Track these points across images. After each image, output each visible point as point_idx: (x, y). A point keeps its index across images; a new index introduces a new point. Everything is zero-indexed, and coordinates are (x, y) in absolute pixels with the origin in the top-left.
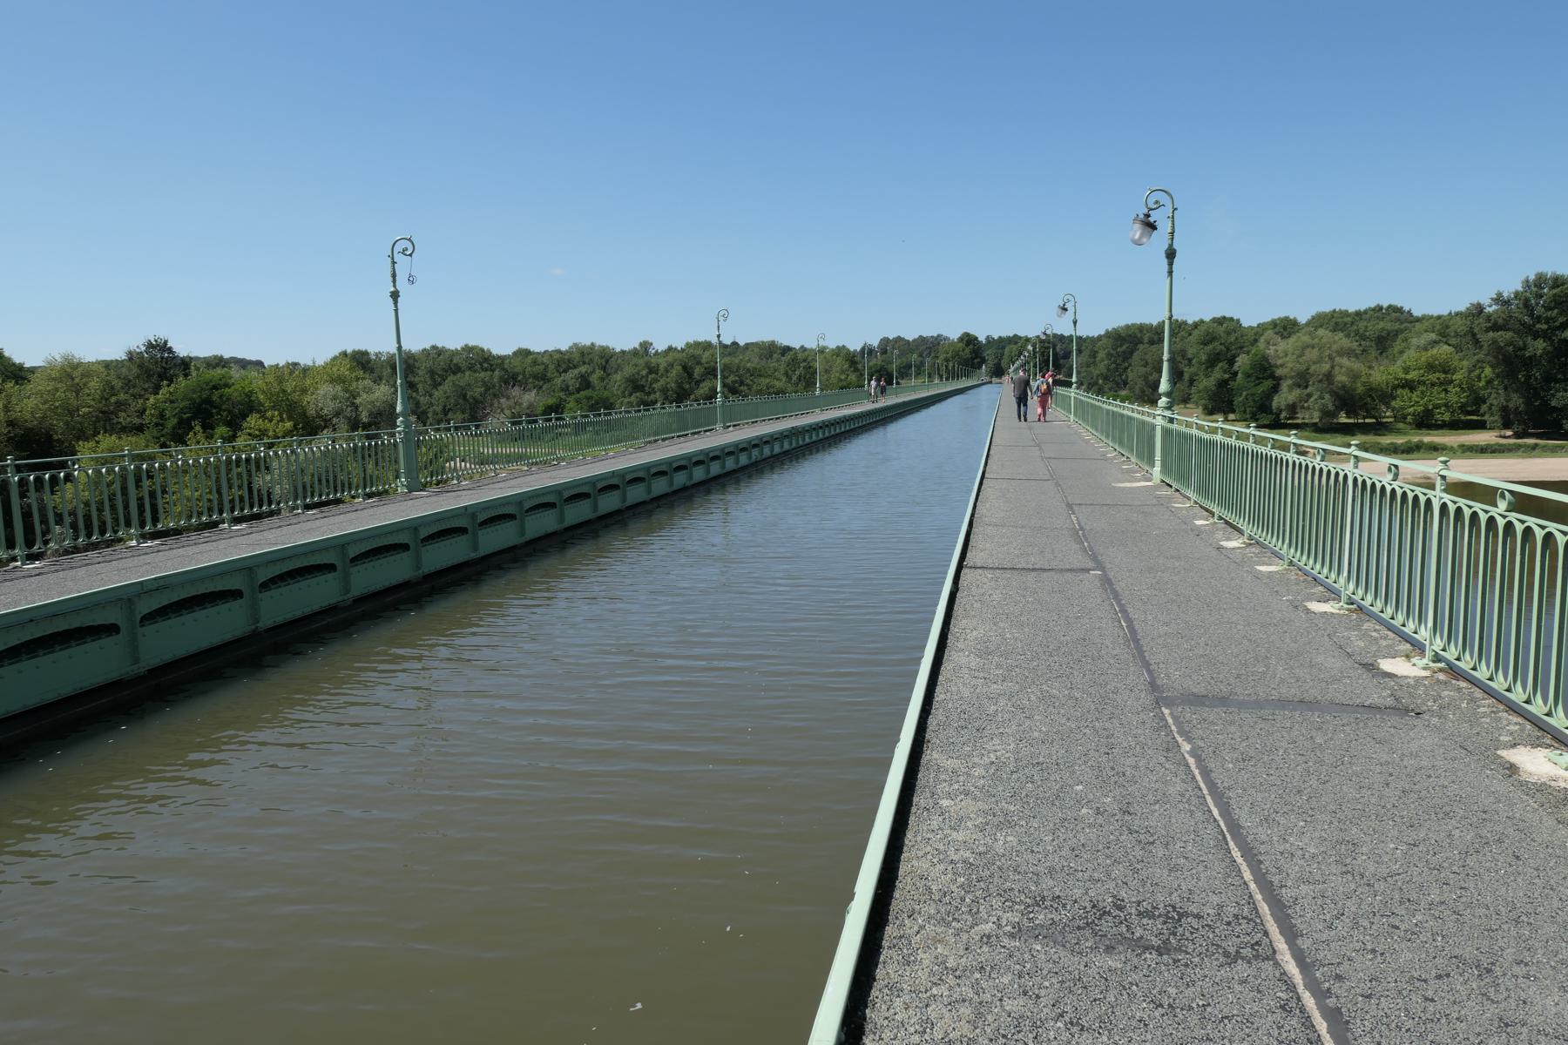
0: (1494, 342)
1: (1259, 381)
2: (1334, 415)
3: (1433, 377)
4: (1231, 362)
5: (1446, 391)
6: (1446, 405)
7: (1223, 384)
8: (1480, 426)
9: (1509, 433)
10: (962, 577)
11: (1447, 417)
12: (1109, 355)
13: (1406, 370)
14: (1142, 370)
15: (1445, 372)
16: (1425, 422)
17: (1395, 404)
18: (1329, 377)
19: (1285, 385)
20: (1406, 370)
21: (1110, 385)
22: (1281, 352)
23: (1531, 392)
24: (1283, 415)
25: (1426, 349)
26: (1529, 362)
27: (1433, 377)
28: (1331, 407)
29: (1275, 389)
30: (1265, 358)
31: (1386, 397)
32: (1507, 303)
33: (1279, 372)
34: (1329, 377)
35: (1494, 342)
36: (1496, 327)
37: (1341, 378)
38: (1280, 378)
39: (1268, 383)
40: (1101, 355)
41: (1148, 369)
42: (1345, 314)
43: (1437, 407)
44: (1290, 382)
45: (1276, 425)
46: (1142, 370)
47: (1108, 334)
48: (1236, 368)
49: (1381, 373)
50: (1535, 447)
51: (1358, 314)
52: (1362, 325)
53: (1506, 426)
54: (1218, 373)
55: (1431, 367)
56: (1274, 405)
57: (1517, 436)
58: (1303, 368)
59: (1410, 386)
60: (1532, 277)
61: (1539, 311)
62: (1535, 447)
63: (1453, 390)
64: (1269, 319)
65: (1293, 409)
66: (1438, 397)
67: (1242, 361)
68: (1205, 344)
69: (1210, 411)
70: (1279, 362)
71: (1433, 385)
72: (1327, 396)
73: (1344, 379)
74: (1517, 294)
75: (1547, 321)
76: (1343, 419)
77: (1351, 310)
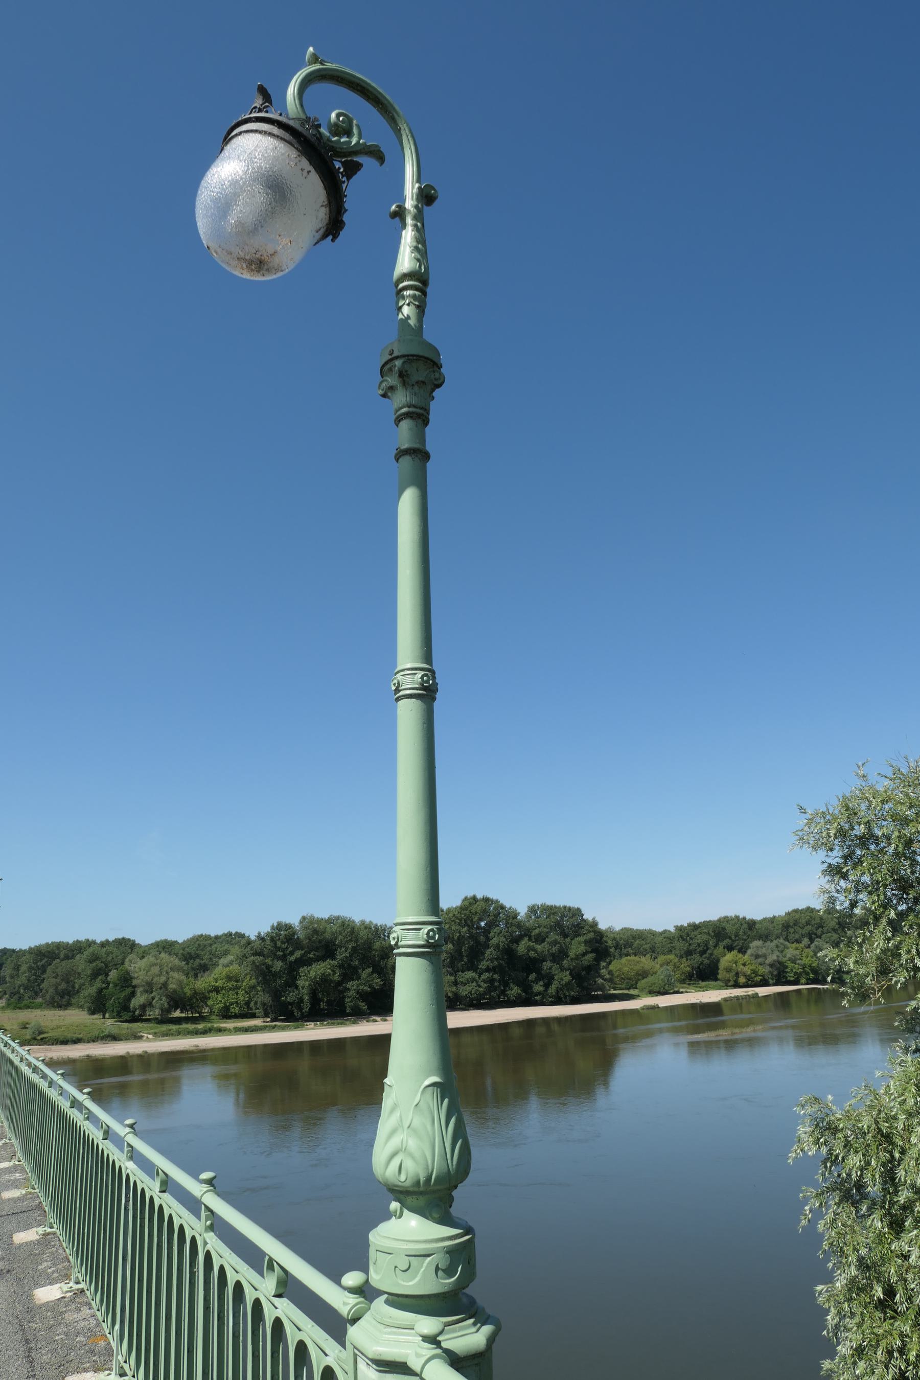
0: (254, 962)
1: (123, 988)
2: (169, 1011)
3: (230, 984)
4: (107, 975)
5: (237, 994)
6: (237, 1002)
7: (100, 991)
8: (253, 1016)
9: (269, 1020)
10: (251, 134)
11: (237, 1010)
12: (30, 968)
13: (216, 980)
14: (53, 981)
15: (237, 981)
16: (226, 1014)
17: (210, 1003)
18: (165, 985)
19: (139, 990)
20: (216, 980)
21: (29, 994)
22: (137, 967)
23: (276, 995)
24: (137, 1013)
25: (227, 966)
26: (275, 975)
27: (230, 984)
28: (166, 1006)
29: (133, 994)
30: (128, 973)
31: (205, 998)
32: (263, 939)
33: (135, 982)
34: (165, 985)
35: (254, 962)
36: (256, 954)
37: (172, 986)
38: (134, 987)
39: (129, 990)
40: (24, 968)
41: (58, 980)
42: (208, 937)
43: (232, 1004)
44: (141, 989)
45: (134, 1020)
46: (53, 981)
47: (31, 951)
48: (109, 978)
49: (203, 983)
50: (274, 1027)
51: (217, 937)
52: (218, 945)
53: (266, 1016)
54: (98, 984)
55: (229, 978)
56: (132, 1005)
57: (272, 1021)
58: (149, 980)
59: (217, 990)
60: (275, 924)
61: (279, 943)
62: (274, 1027)
63: (241, 992)
64: (153, 941)
65: (143, 1007)
66: (232, 997)
67: (113, 975)
68: (91, 962)
69: (93, 1012)
70: (136, 975)
71: (230, 989)
72: (164, 998)
73: (174, 986)
74: (267, 934)
75: (283, 950)
76: (177, 1014)
77: (213, 935)
